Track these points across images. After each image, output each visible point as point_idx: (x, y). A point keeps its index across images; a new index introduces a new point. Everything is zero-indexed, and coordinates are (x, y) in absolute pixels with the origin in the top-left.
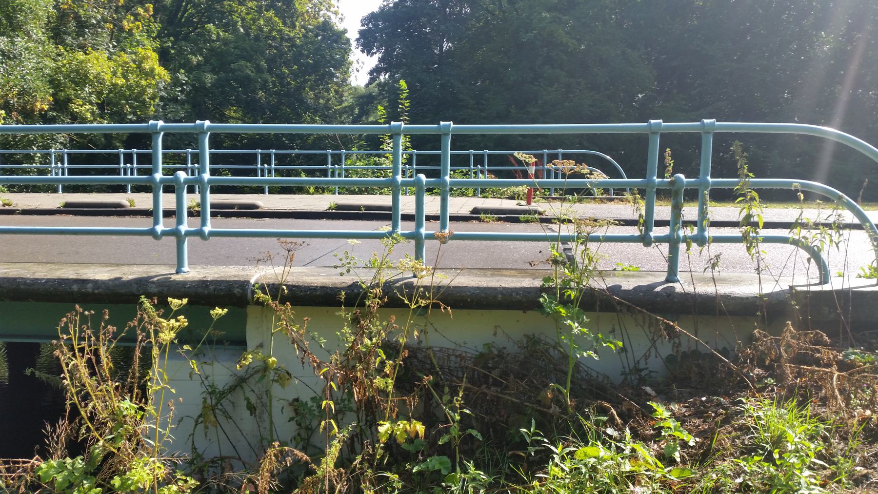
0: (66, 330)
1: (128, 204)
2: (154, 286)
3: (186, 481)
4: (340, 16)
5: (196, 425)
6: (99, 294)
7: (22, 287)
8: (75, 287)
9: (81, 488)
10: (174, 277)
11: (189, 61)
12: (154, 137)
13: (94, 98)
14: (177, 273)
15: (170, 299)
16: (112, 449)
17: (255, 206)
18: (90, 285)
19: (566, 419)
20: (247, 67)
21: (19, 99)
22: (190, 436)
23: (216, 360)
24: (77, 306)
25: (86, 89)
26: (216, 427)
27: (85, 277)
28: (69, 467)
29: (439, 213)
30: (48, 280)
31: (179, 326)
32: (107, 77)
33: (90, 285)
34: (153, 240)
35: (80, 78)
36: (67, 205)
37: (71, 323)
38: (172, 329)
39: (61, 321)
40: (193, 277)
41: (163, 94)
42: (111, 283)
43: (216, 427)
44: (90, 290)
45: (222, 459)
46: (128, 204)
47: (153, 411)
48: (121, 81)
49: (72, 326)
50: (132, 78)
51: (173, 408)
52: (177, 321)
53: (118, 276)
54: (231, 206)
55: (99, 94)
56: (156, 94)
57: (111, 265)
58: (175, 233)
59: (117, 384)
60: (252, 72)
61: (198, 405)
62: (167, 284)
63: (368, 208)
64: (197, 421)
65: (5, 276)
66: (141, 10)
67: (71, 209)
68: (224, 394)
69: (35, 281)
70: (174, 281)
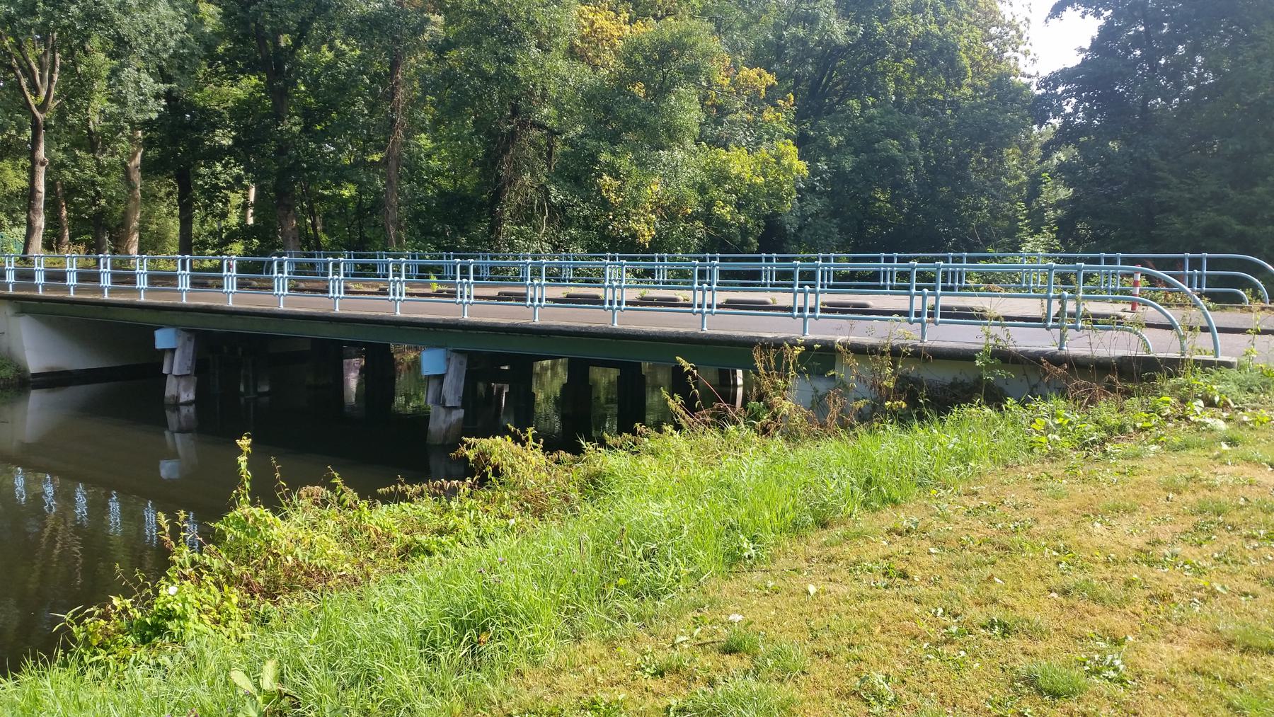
4: (1032, 56)
11: (827, 143)
17: (865, 306)
19: (651, 212)
20: (893, 145)
29: (792, 305)
32: (747, 176)
35: (721, 177)
36: (728, 301)
48: (760, 180)
50: (772, 173)
54: (847, 305)
58: (803, 316)
60: (899, 151)
63: (960, 309)
66: (781, 102)
67: (730, 304)
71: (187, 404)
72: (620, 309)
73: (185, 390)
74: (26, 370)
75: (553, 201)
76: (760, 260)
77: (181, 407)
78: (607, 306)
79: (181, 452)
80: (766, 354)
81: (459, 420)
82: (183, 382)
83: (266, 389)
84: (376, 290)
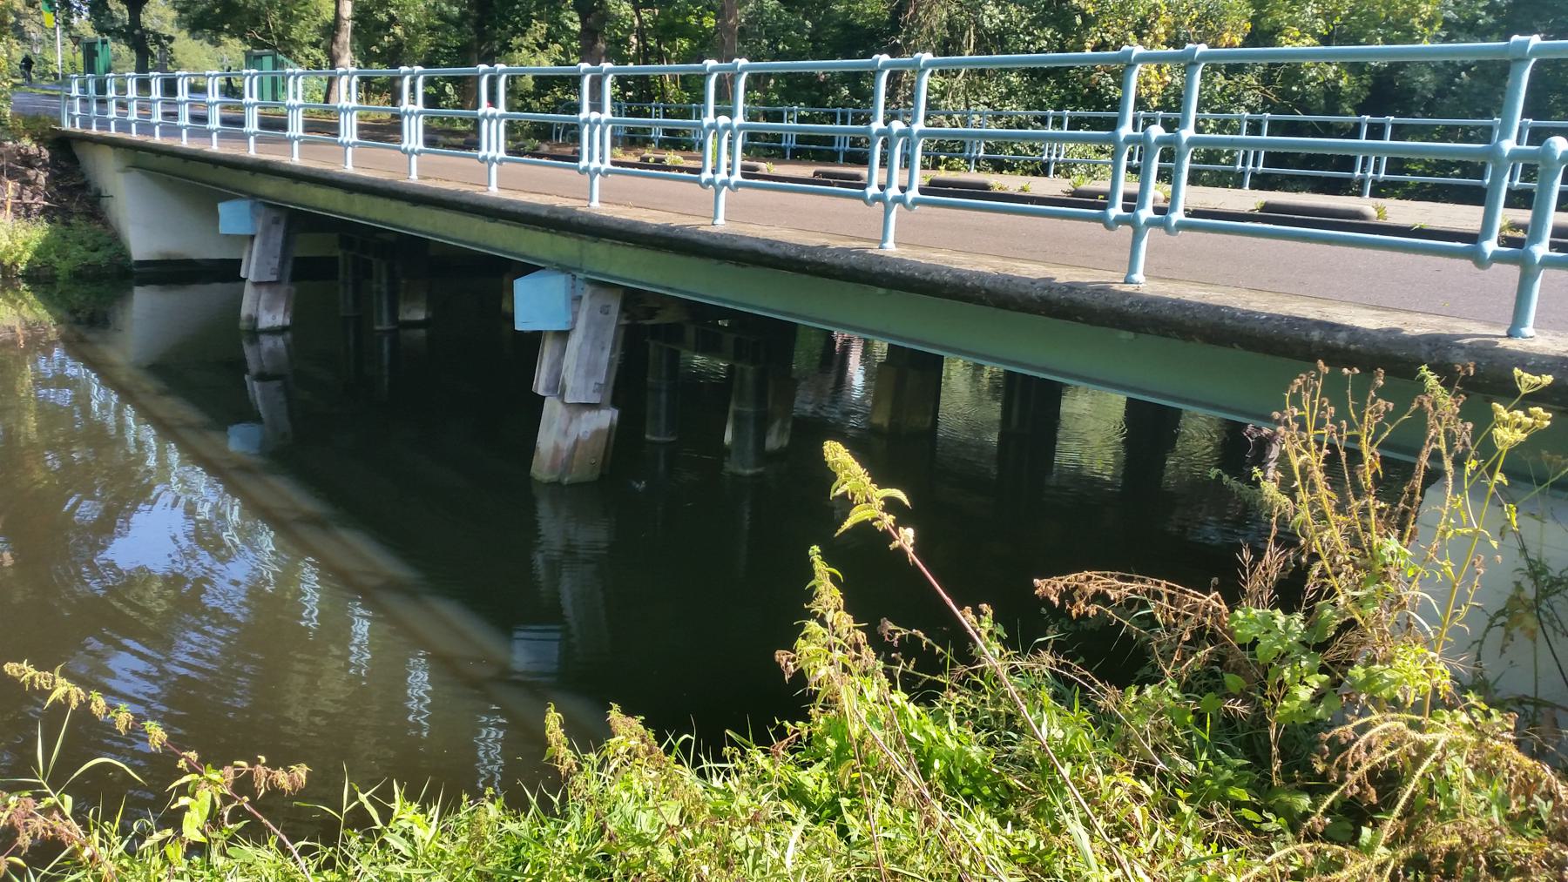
0: (1296, 400)
1: (1375, 214)
2: (1462, 352)
3: (1488, 715)
5: (1490, 627)
6: (1357, 352)
7: (1228, 322)
8: (1316, 335)
9: (1296, 667)
10: (1505, 343)
12: (1514, 67)
13: (1320, 25)
14: (1509, 336)
15: (1517, 371)
16: (1357, 617)
18: (1342, 335)
21: (1199, 28)
22: (1474, 643)
23: (1554, 518)
24: (1321, 363)
25: (1309, 9)
26: (1534, 641)
27: (1335, 319)
28: (1280, 627)
30: (1271, 317)
31: (1533, 424)
33: (1342, 335)
34: (1475, 269)
36: (1267, 207)
37: (1306, 390)
38: (1519, 425)
39: (1293, 384)
40: (1544, 349)
41: (1450, 14)
42: (1380, 335)
43: (1534, 641)
44: (1342, 343)
45: (1537, 703)
46: (1375, 214)
47: (1450, 569)
49: (1308, 395)
51: (1482, 571)
52: (1528, 415)
53: (1395, 325)
55: (1329, 16)
56: (1438, 14)
57: (1377, 307)
59: (1383, 505)
61: (1499, 593)
62: (1489, 353)
64: (1492, 620)
65: (1203, 301)
67: (1270, 213)
68: (1560, 584)
69: (1249, 316)
70: (1504, 349)
71: (272, 331)
72: (1164, 225)
73: (269, 309)
74: (128, 257)
75: (987, 24)
76: (1354, 132)
77: (263, 338)
78: (1116, 211)
79: (264, 415)
80: (1342, 413)
81: (597, 433)
82: (265, 295)
83: (420, 315)
84: (636, 160)
